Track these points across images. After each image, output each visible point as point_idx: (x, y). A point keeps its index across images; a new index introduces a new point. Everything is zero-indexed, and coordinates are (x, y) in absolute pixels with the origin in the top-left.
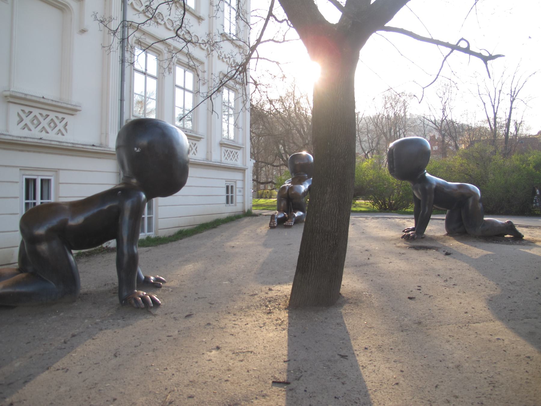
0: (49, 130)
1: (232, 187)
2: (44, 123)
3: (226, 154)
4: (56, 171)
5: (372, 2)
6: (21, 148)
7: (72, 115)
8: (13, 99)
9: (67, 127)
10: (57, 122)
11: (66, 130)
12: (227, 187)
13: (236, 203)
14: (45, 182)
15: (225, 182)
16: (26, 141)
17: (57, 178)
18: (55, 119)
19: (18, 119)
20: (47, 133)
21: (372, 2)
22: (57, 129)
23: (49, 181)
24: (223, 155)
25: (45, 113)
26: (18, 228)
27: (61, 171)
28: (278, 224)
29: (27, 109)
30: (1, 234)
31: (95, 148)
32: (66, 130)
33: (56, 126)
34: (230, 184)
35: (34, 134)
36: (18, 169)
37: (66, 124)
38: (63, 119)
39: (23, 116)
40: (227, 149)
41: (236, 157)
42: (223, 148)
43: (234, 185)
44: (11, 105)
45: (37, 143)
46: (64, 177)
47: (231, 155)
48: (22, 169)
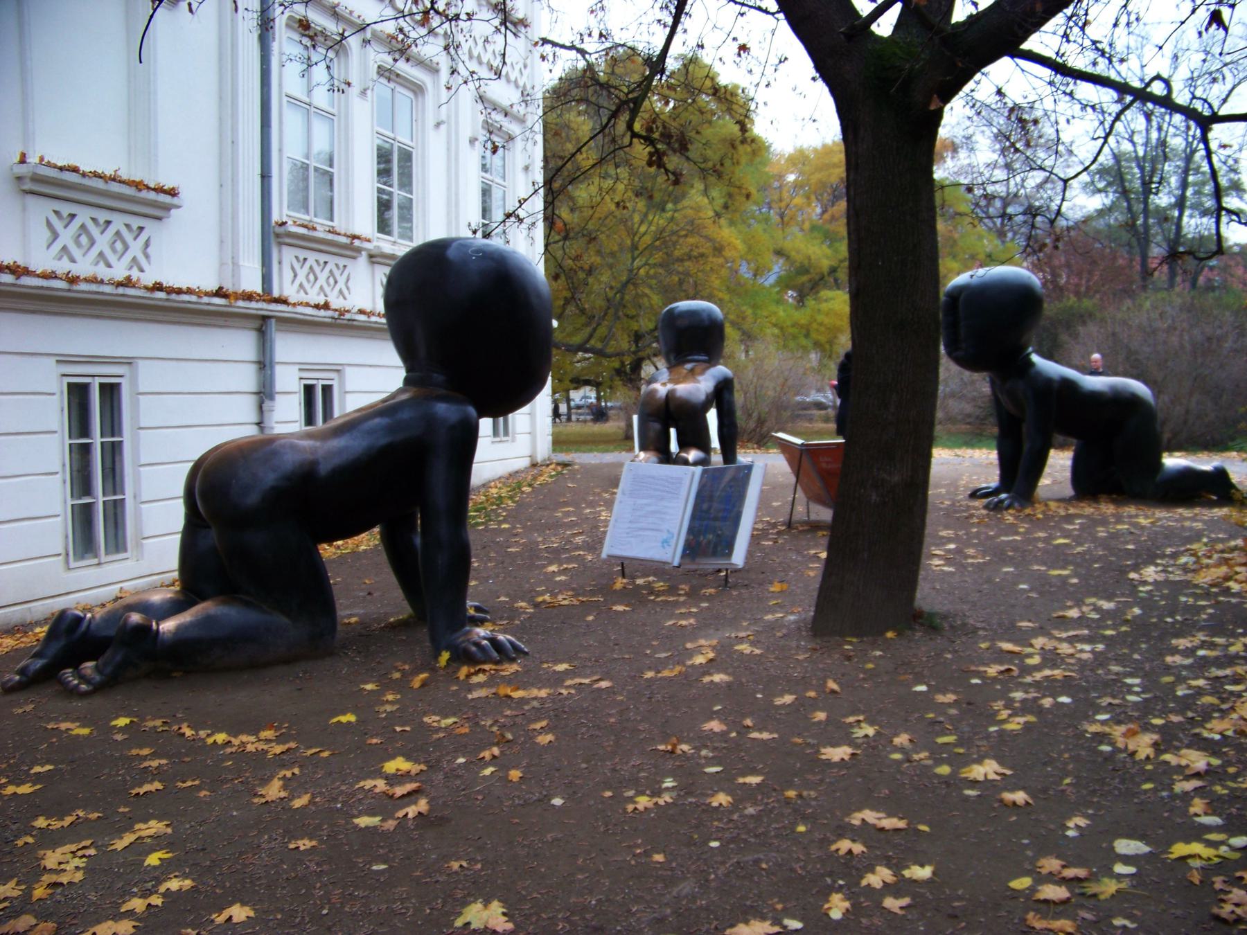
0: (112, 258)
1: (327, 390)
2: (103, 242)
3: (302, 274)
5: (960, 13)
6: (137, 314)
7: (159, 219)
8: (51, 186)
9: (149, 250)
10: (95, 231)
11: (147, 256)
12: (309, 390)
13: (514, 433)
15: (298, 374)
16: (102, 293)
17: (342, 383)
19: (47, 234)
20: (109, 266)
21: (960, 13)
25: (103, 216)
26: (180, 489)
27: (141, 362)
29: (66, 209)
31: (253, 305)
32: (147, 256)
34: (95, 375)
36: (54, 359)
37: (147, 244)
38: (141, 229)
39: (95, 231)
40: (302, 254)
41: (341, 284)
42: (377, 267)
44: (30, 198)
45: (42, 288)
46: (149, 376)
48: (63, 360)
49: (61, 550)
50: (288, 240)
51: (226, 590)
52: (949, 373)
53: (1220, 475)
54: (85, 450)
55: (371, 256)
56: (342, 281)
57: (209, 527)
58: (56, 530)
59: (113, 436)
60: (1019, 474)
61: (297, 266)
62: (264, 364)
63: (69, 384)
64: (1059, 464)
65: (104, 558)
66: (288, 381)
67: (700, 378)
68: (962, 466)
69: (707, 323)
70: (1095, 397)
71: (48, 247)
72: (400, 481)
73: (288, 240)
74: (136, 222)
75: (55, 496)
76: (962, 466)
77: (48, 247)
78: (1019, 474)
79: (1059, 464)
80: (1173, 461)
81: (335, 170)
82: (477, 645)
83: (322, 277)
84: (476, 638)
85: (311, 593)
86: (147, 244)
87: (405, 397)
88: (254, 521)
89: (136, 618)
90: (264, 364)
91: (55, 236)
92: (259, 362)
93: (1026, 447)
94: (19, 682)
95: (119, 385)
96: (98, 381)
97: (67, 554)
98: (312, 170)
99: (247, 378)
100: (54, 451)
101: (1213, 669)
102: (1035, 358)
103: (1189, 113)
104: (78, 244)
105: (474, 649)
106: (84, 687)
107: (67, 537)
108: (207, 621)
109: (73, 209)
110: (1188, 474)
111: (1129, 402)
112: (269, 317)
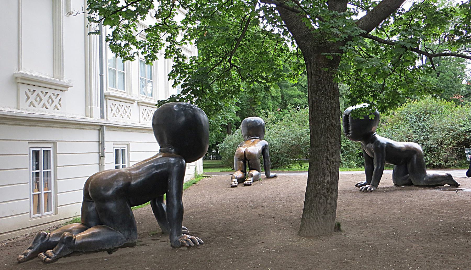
1: (47, 153)
3: (145, 114)
4: (54, 143)
9: (61, 102)
10: (53, 97)
11: (60, 105)
12: (117, 151)
14: (47, 153)
18: (40, 93)
22: (42, 103)
23: (125, 150)
24: (141, 115)
25: (45, 90)
28: (239, 183)
29: (32, 88)
30: (1, 204)
32: (60, 105)
33: (41, 100)
34: (41, 148)
35: (26, 110)
40: (114, 102)
41: (128, 113)
43: (126, 149)
47: (145, 114)
49: (29, 211)
50: (109, 98)
51: (99, 223)
52: (346, 141)
53: (450, 176)
54: (37, 174)
55: (138, 103)
56: (128, 111)
57: (93, 202)
58: (27, 205)
59: (47, 169)
60: (373, 176)
61: (112, 107)
62: (101, 143)
63: (33, 151)
64: (388, 175)
65: (44, 214)
66: (109, 149)
67: (256, 145)
68: (351, 176)
69: (259, 124)
70: (399, 150)
71: (26, 101)
72: (158, 185)
73: (109, 98)
74: (56, 92)
75: (27, 191)
76: (351, 176)
77: (26, 101)
78: (373, 176)
79: (388, 175)
80: (430, 173)
81: (125, 72)
82: (186, 240)
83: (122, 110)
84: (185, 238)
85: (129, 223)
86: (60, 100)
87: (159, 156)
88: (110, 201)
89: (67, 234)
90: (101, 143)
91: (28, 98)
92: (99, 142)
93: (375, 167)
94: (24, 258)
95: (50, 151)
96: (43, 149)
97: (31, 212)
98: (117, 72)
99: (95, 147)
100: (27, 174)
101: (221, 163)
102: (377, 136)
103: (426, 54)
104: (36, 101)
105: (185, 242)
106: (48, 259)
107: (31, 206)
108: (93, 235)
109: (35, 88)
110: (436, 177)
111: (415, 151)
112: (103, 126)
